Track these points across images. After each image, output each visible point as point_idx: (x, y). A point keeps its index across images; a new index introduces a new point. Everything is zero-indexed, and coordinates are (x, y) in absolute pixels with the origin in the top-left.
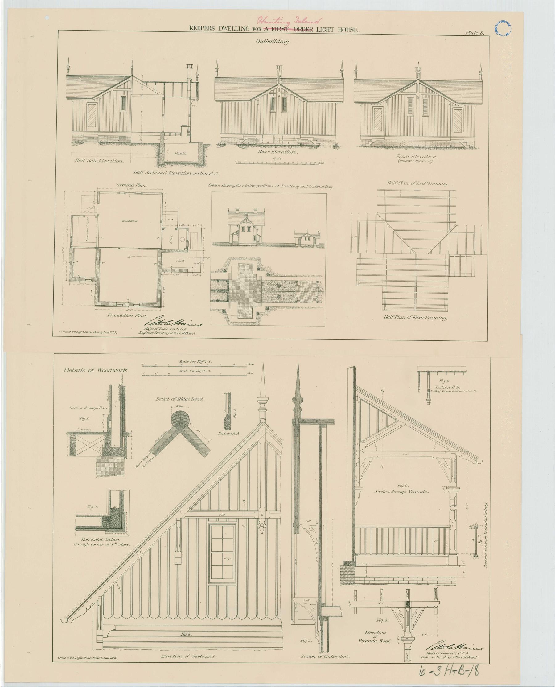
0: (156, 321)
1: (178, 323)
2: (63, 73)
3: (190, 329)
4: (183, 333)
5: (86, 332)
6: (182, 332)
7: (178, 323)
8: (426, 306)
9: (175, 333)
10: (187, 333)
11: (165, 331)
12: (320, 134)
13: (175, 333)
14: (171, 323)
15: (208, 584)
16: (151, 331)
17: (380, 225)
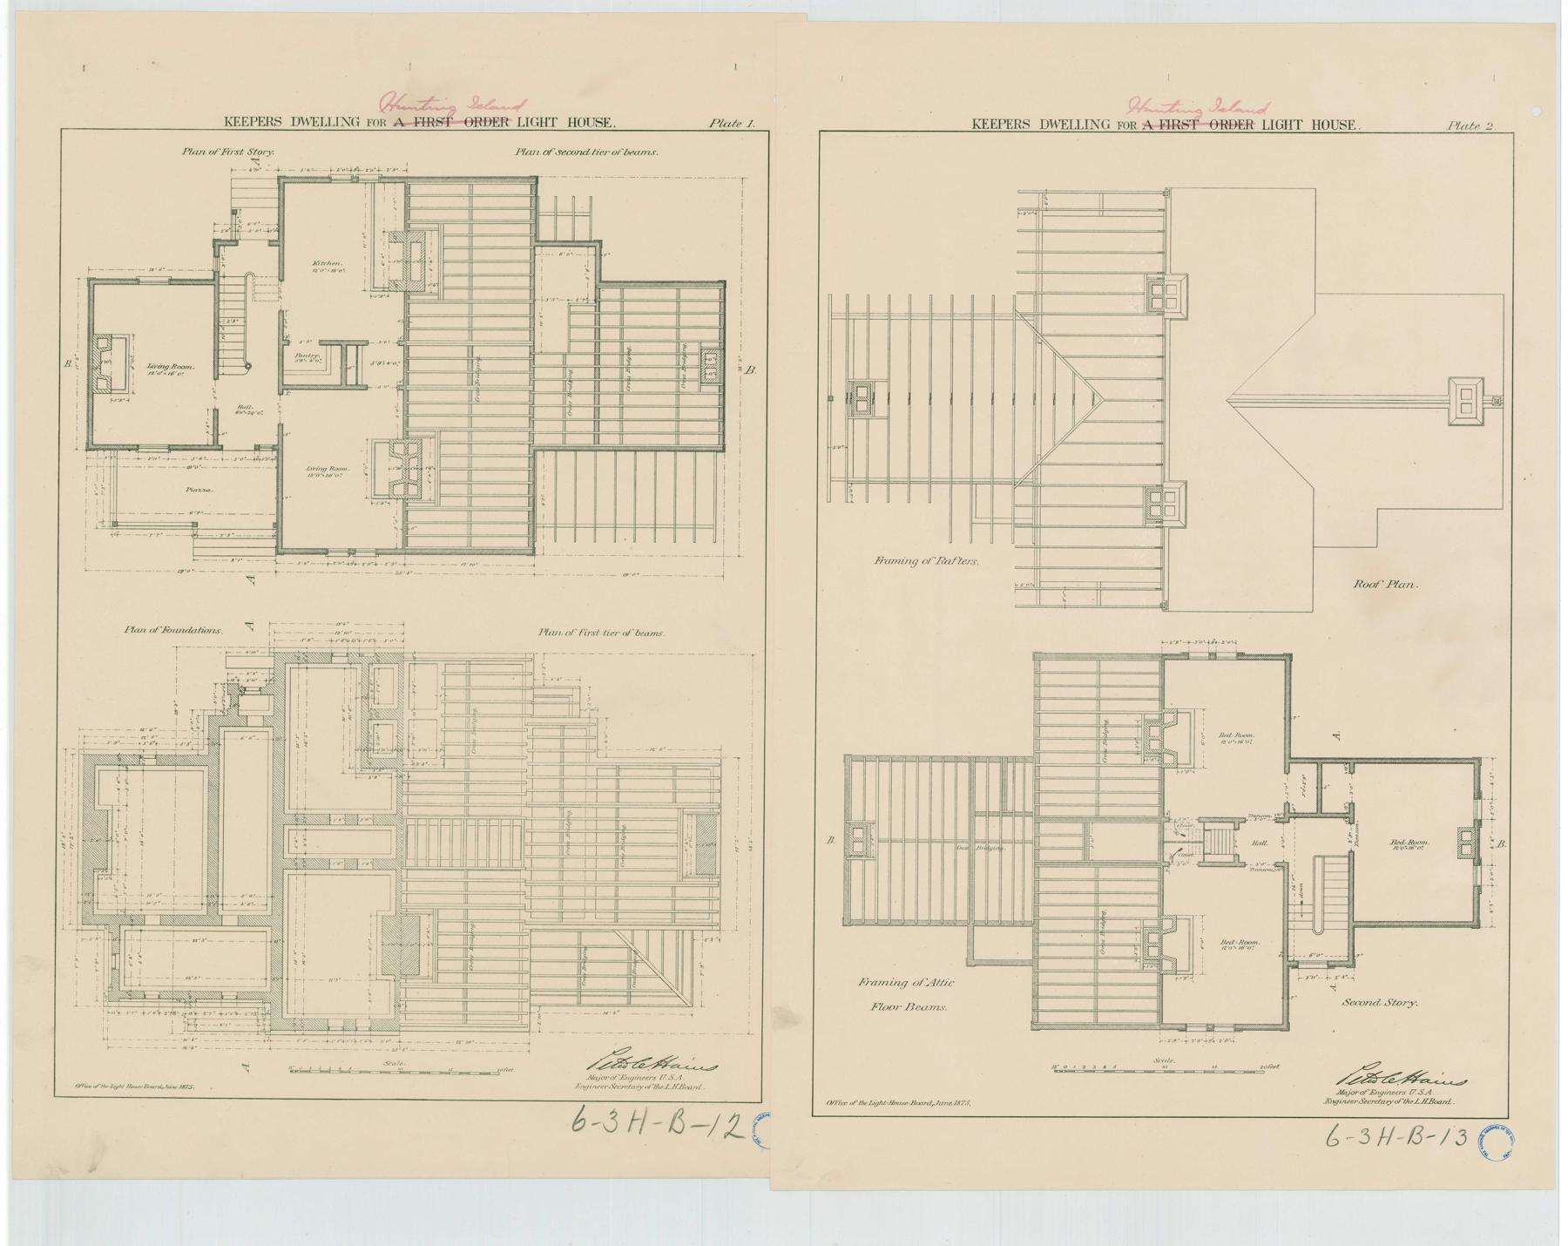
1: (1413, 1078)
4: (1425, 1101)
6: (672, 1083)
7: (1413, 1078)
8: (216, 551)
9: (657, 1087)
10: (683, 1087)
11: (1384, 1098)
12: (242, 297)
13: (657, 1087)
14: (1397, 1078)
16: (1351, 1098)
17: (1048, 475)
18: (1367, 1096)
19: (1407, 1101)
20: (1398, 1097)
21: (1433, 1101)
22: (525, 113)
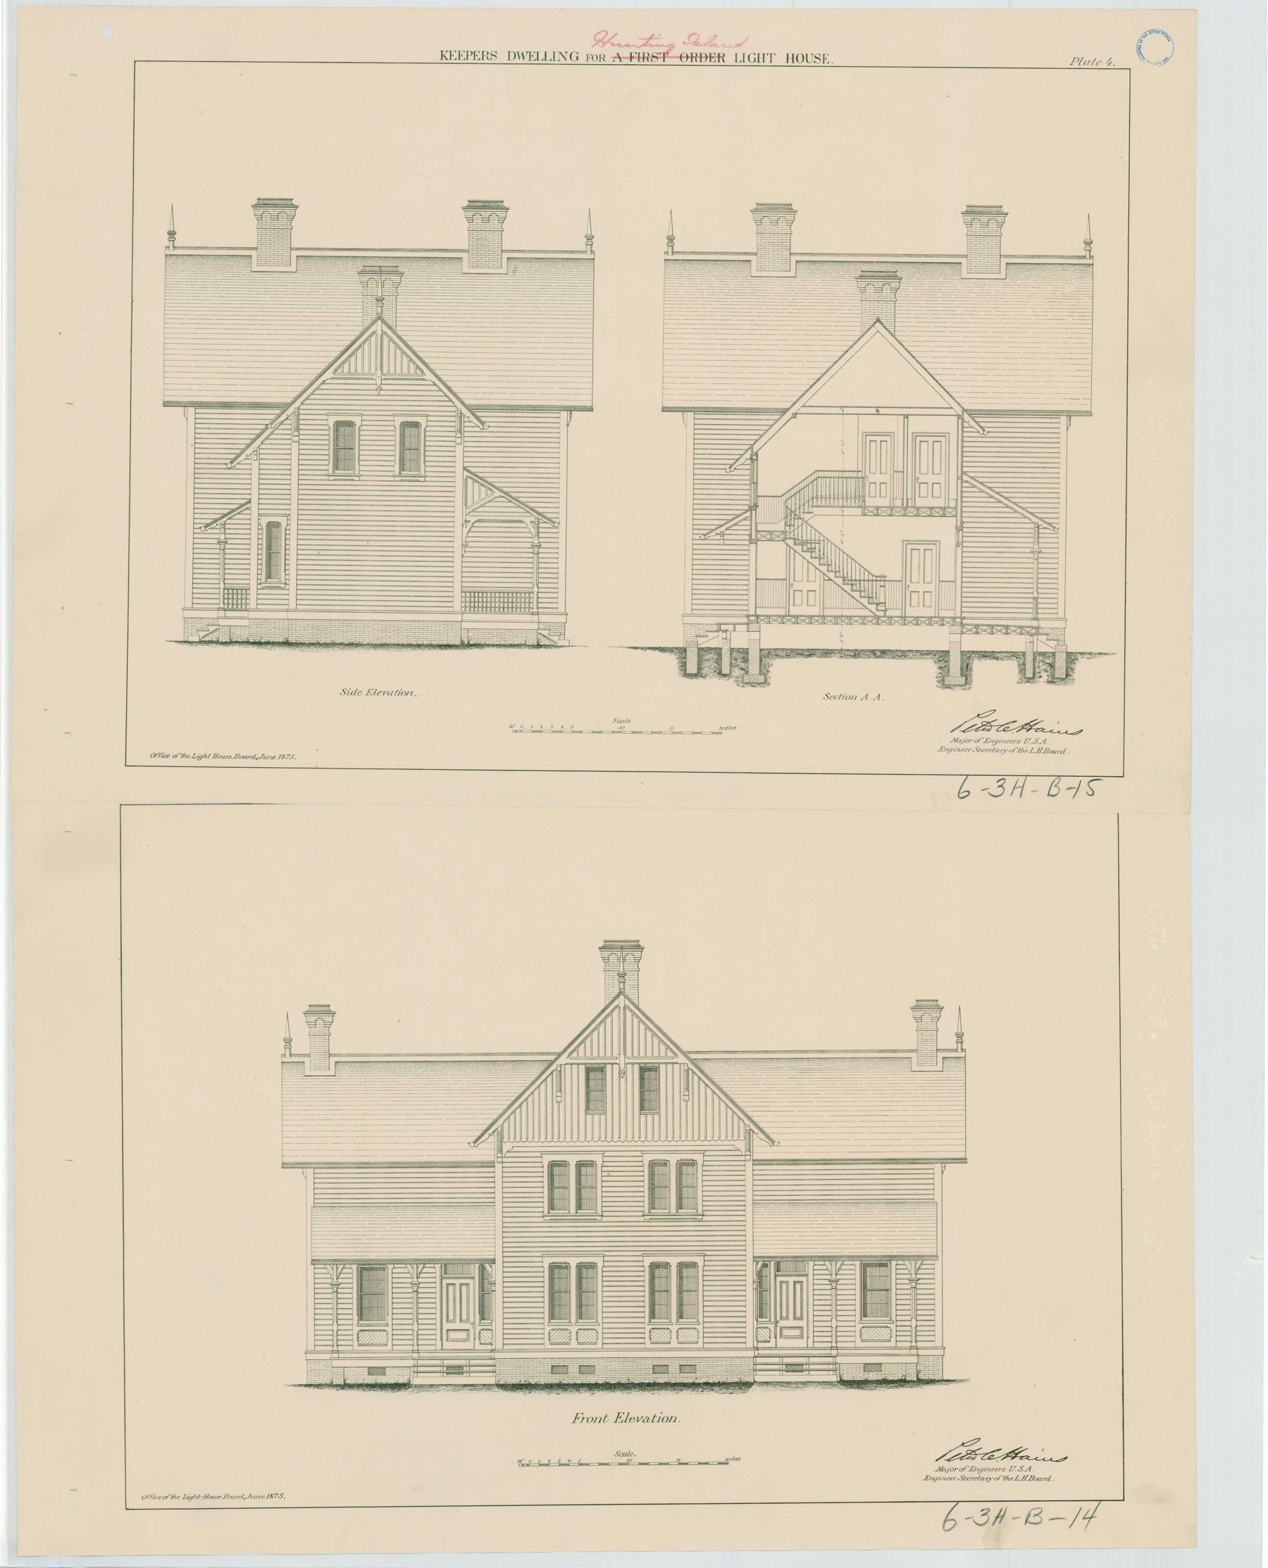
0: (978, 722)
1: (1028, 727)
2: (153, 245)
3: (1055, 742)
4: (1039, 751)
5: (216, 756)
6: (1036, 747)
7: (1028, 727)
9: (1021, 750)
11: (998, 746)
14: (1012, 726)
15: (446, 1326)
18: (981, 745)
19: (1021, 750)
21: (1047, 751)
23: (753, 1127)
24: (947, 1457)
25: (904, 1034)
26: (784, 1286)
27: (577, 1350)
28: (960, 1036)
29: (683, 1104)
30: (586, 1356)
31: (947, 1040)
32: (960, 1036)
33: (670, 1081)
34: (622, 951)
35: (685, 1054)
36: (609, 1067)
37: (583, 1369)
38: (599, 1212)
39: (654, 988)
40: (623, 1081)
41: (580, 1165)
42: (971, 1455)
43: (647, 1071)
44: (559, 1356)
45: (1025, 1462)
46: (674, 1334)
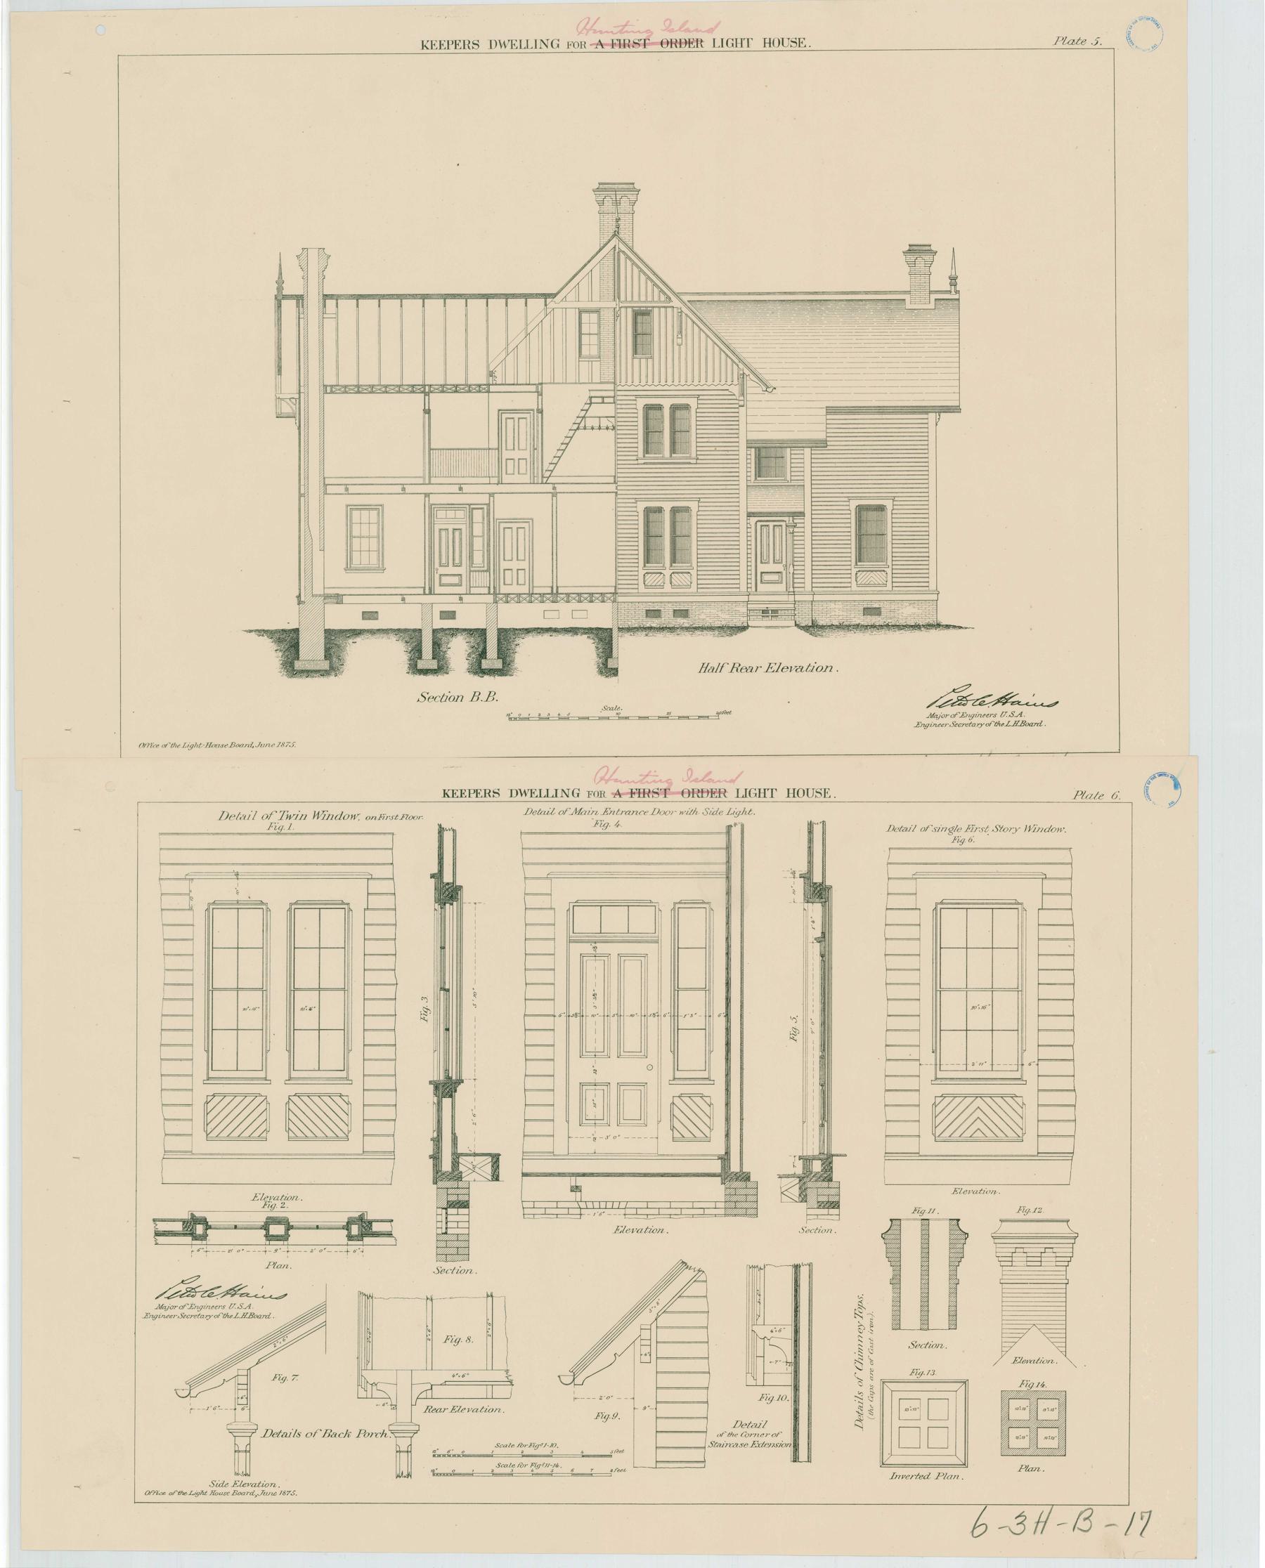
15: (761, 568)
16: (169, 1312)
18: (186, 1311)
20: (988, 720)
22: (742, 785)
23: (747, 372)
24: (939, 703)
25: (896, 277)
26: (443, 533)
27: (671, 595)
28: (953, 280)
29: (676, 347)
30: (682, 601)
31: (940, 281)
32: (953, 280)
33: (662, 324)
34: (615, 195)
35: (677, 295)
36: (656, 310)
37: (677, 613)
38: (694, 455)
39: (647, 236)
40: (329, 325)
41: (674, 408)
42: (962, 701)
43: (641, 314)
44: (653, 601)
45: (1017, 708)
46: (668, 577)
